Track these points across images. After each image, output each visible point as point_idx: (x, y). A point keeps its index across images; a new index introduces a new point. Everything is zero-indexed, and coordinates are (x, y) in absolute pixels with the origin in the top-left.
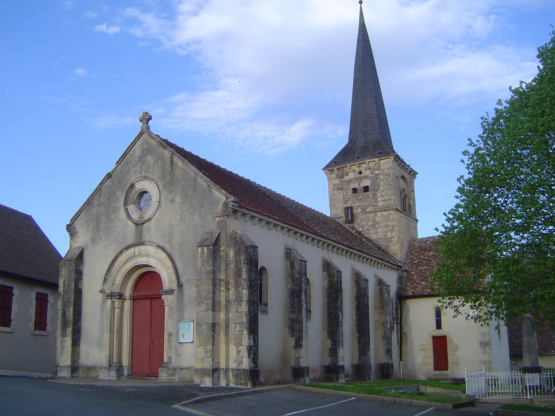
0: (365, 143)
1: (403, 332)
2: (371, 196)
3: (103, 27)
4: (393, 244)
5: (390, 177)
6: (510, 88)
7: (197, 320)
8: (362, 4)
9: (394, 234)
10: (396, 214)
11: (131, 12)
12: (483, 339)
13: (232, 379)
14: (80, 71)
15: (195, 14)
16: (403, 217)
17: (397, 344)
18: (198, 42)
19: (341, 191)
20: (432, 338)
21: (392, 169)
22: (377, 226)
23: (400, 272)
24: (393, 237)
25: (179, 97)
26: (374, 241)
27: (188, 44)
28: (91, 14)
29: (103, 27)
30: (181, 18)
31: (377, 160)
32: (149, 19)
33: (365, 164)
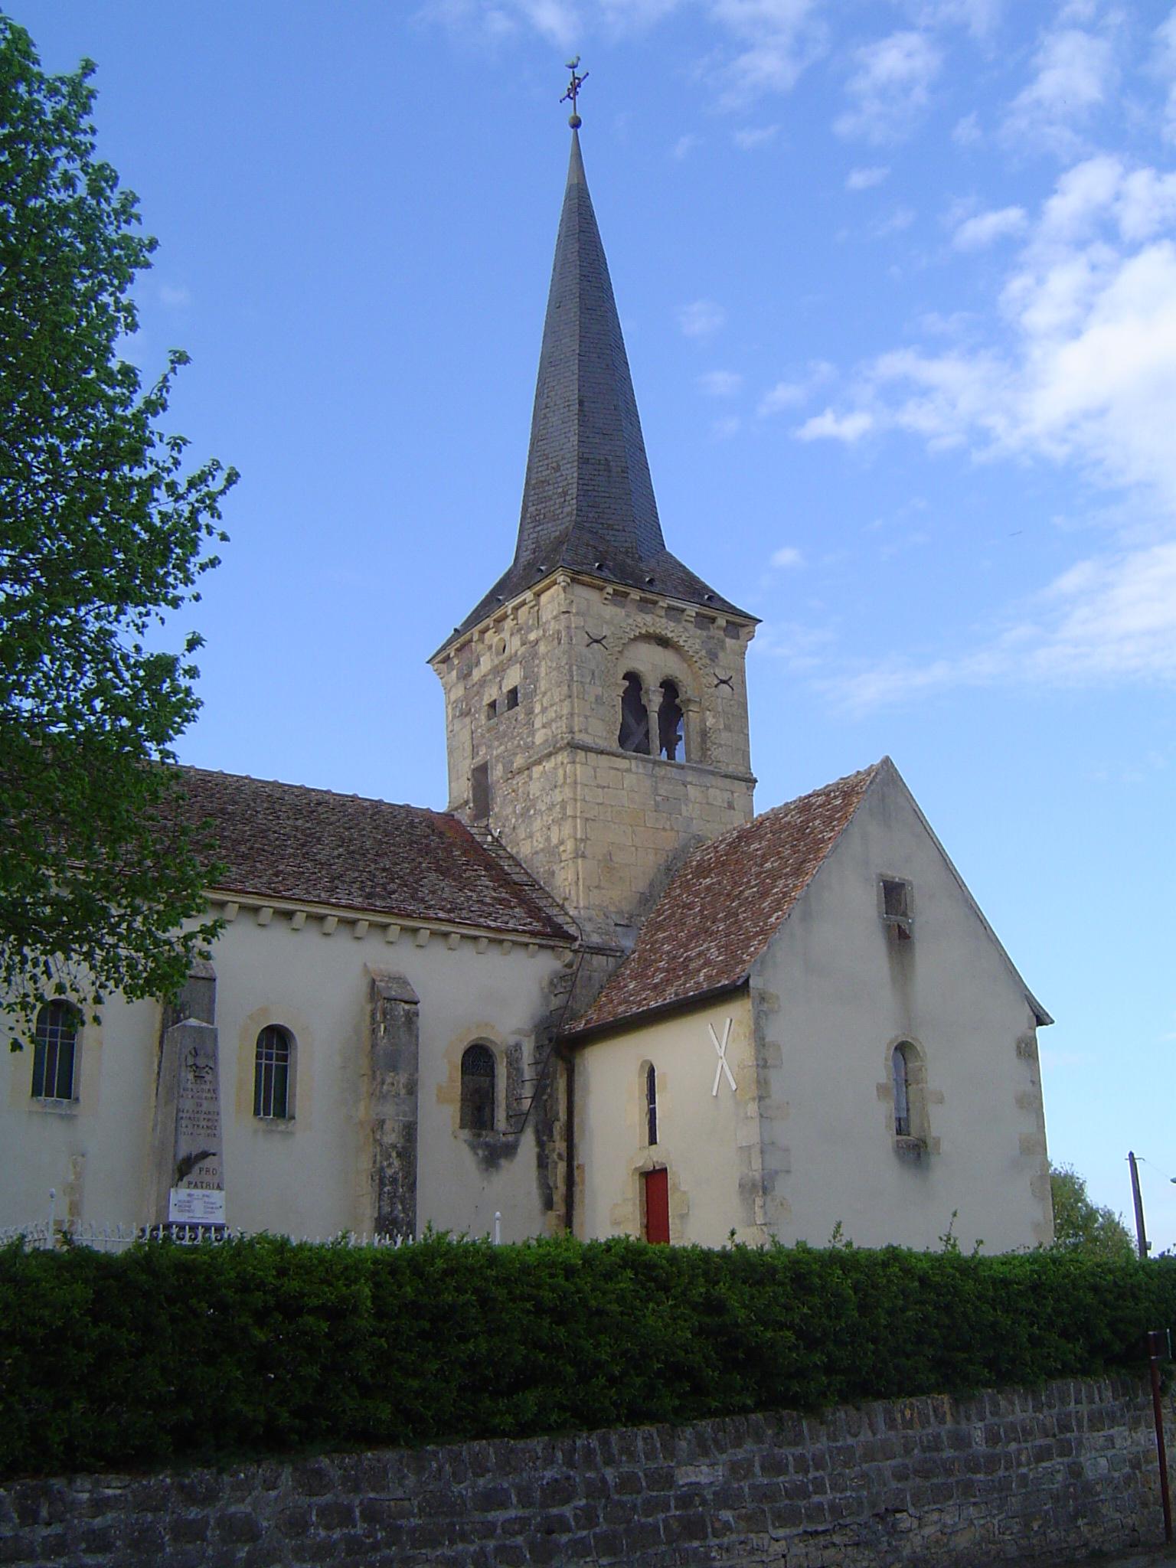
0: (534, 553)
1: (576, 1163)
2: (521, 717)
3: (824, 425)
4: (563, 864)
5: (559, 643)
6: (139, 220)
7: (755, 1213)
8: (579, 130)
9: (567, 829)
10: (574, 762)
11: (896, 363)
12: (747, 1171)
13: (572, 1370)
14: (787, 556)
15: (1074, 332)
16: (629, 770)
17: (536, 1201)
18: (1099, 413)
19: (467, 720)
20: (637, 1177)
21: (567, 615)
22: (532, 812)
23: (568, 956)
24: (562, 843)
25: (1072, 580)
26: (525, 862)
27: (1072, 426)
28: (786, 394)
29: (824, 425)
30: (1036, 352)
31: (528, 595)
32: (946, 372)
33: (509, 620)
